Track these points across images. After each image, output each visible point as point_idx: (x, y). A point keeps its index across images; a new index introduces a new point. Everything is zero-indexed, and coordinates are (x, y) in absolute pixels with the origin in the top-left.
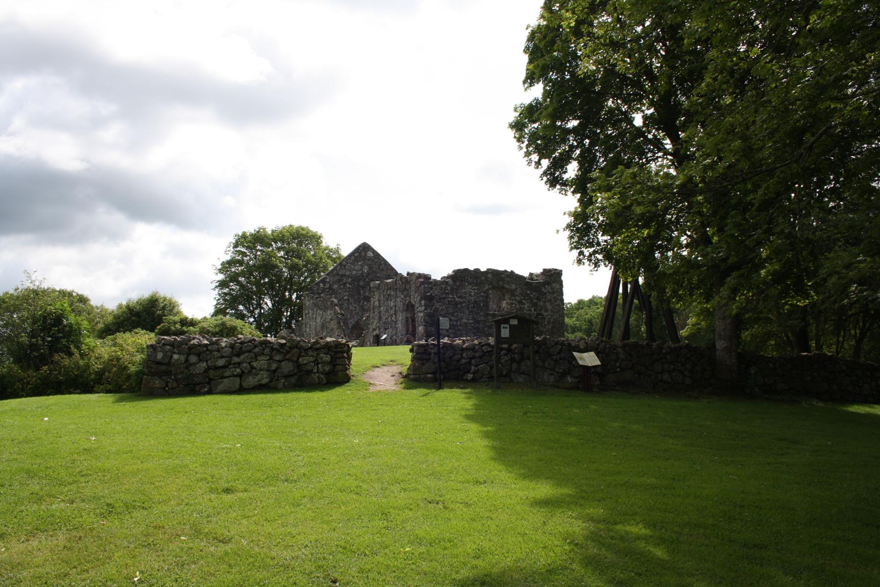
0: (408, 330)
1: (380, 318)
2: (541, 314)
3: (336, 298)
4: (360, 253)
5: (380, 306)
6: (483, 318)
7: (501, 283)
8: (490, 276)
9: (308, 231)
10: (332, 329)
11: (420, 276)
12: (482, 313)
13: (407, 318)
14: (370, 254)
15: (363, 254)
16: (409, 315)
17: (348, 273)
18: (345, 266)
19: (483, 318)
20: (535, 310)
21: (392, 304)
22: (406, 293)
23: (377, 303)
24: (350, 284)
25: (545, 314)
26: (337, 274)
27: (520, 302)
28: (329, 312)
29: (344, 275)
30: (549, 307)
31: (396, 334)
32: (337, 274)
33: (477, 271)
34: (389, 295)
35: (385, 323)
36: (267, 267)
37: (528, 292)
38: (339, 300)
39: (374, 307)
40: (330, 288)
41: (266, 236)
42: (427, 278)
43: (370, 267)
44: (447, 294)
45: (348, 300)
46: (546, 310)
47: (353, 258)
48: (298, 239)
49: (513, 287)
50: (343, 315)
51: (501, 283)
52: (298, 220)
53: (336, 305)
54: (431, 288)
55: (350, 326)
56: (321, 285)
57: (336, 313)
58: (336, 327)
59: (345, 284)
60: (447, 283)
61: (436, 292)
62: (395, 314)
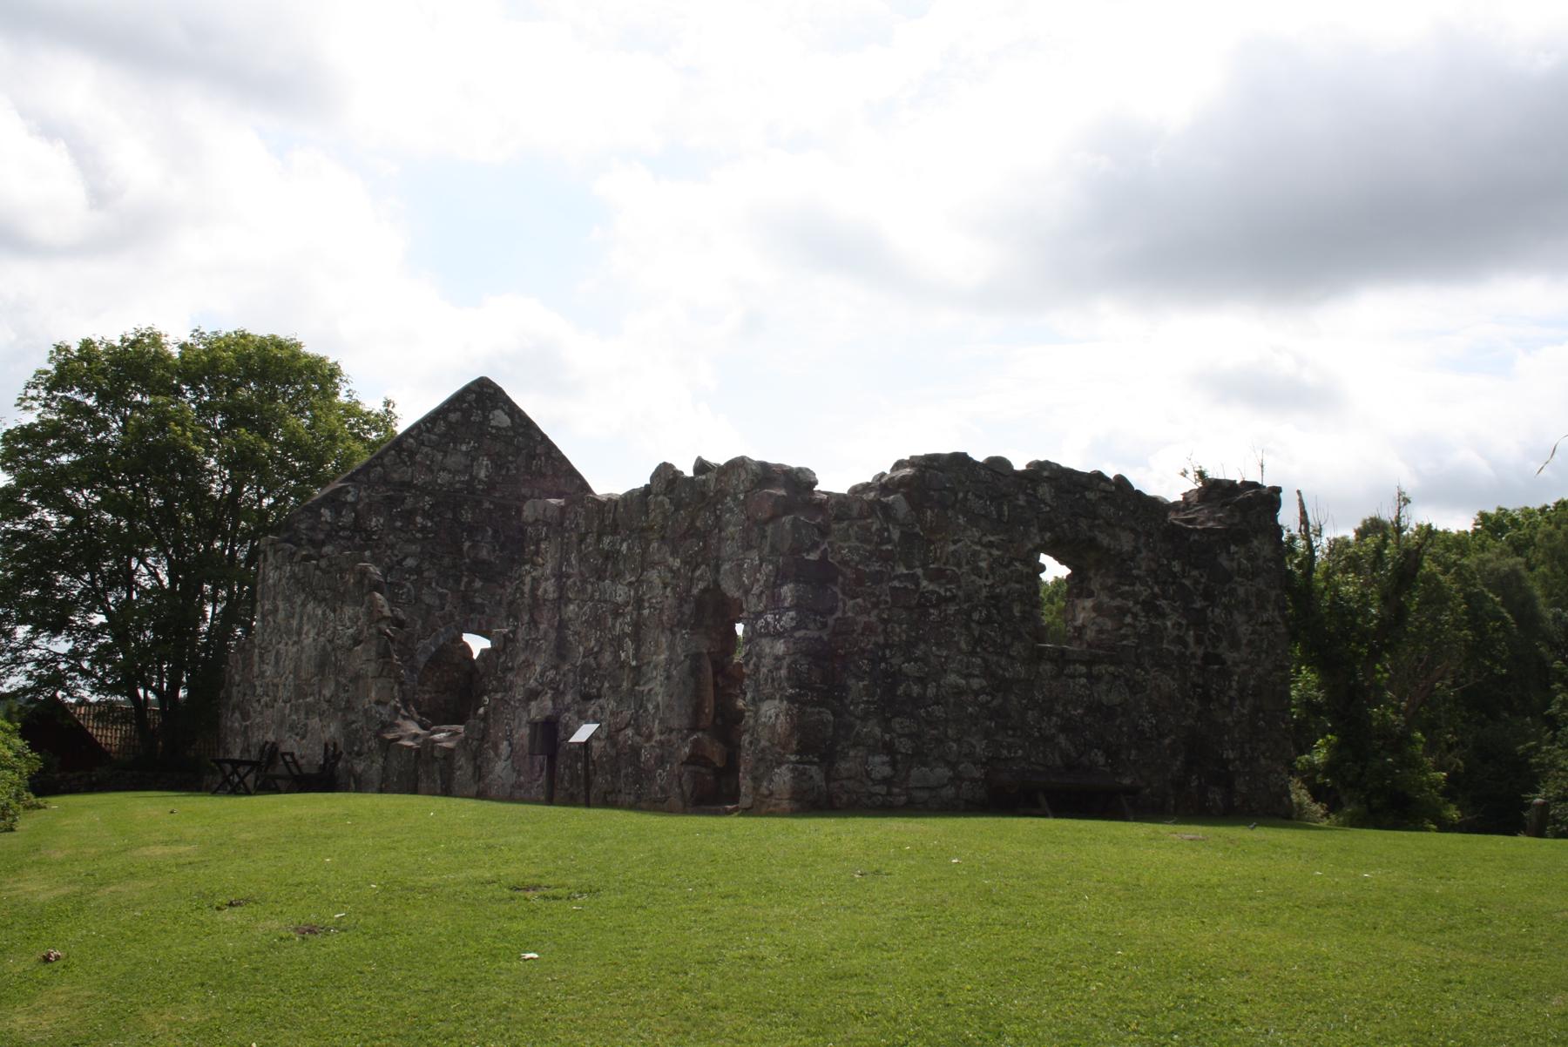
0: (697, 710)
1: (561, 651)
2: (1218, 659)
3: (376, 561)
4: (467, 414)
5: (562, 600)
6: (1021, 670)
7: (1083, 524)
8: (1045, 491)
9: (294, 351)
10: (357, 678)
11: (767, 474)
12: (1017, 649)
13: (696, 658)
14: (501, 419)
15: (476, 417)
16: (704, 645)
17: (421, 479)
18: (412, 454)
19: (1021, 670)
20: (1199, 641)
21: (621, 593)
22: (696, 546)
23: (549, 588)
24: (426, 515)
25: (1231, 656)
26: (384, 480)
27: (1150, 607)
28: (349, 611)
29: (407, 485)
30: (1244, 630)
31: (636, 723)
32: (384, 480)
33: (998, 465)
34: (607, 556)
35: (585, 670)
36: (156, 458)
37: (1176, 566)
38: (388, 571)
39: (536, 603)
40: (358, 527)
41: (161, 358)
42: (800, 481)
43: (498, 464)
44: (886, 558)
45: (418, 570)
46: (1235, 645)
47: (441, 427)
48: (264, 381)
49: (1126, 542)
50: (400, 624)
51: (1083, 524)
52: (262, 321)
53: (377, 587)
54: (824, 531)
55: (422, 659)
56: (326, 514)
57: (374, 617)
58: (371, 668)
59: (408, 516)
60: (886, 508)
61: (845, 547)
62: (637, 637)
